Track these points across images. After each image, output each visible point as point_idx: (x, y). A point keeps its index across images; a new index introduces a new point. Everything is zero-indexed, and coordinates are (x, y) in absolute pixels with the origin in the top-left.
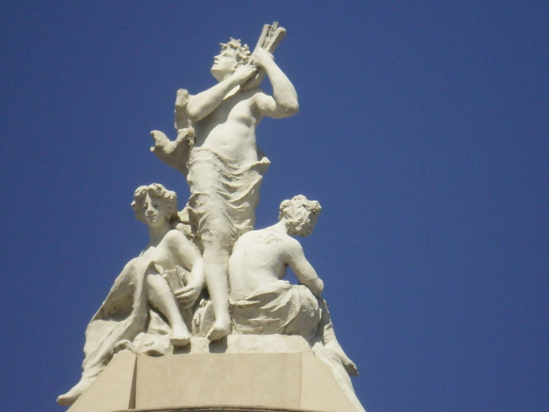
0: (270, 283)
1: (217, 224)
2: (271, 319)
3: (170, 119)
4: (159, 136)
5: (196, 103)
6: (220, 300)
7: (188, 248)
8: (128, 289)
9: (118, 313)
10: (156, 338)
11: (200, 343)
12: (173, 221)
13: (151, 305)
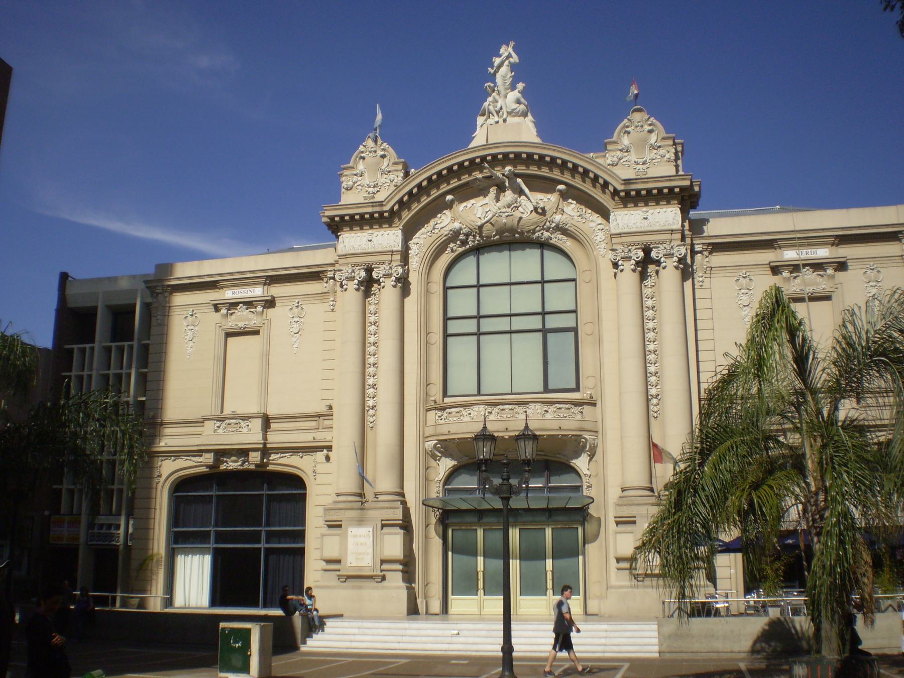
0: (515, 106)
1: (503, 92)
2: (123, 512)
3: (492, 65)
4: (490, 69)
5: (497, 61)
6: (504, 110)
7: (497, 97)
8: (484, 110)
9: (483, 115)
10: (491, 121)
11: (501, 121)
12: (494, 91)
13: (490, 112)
